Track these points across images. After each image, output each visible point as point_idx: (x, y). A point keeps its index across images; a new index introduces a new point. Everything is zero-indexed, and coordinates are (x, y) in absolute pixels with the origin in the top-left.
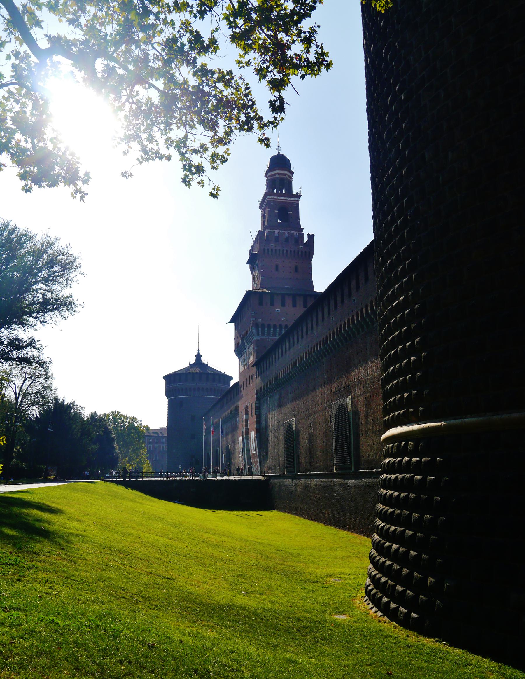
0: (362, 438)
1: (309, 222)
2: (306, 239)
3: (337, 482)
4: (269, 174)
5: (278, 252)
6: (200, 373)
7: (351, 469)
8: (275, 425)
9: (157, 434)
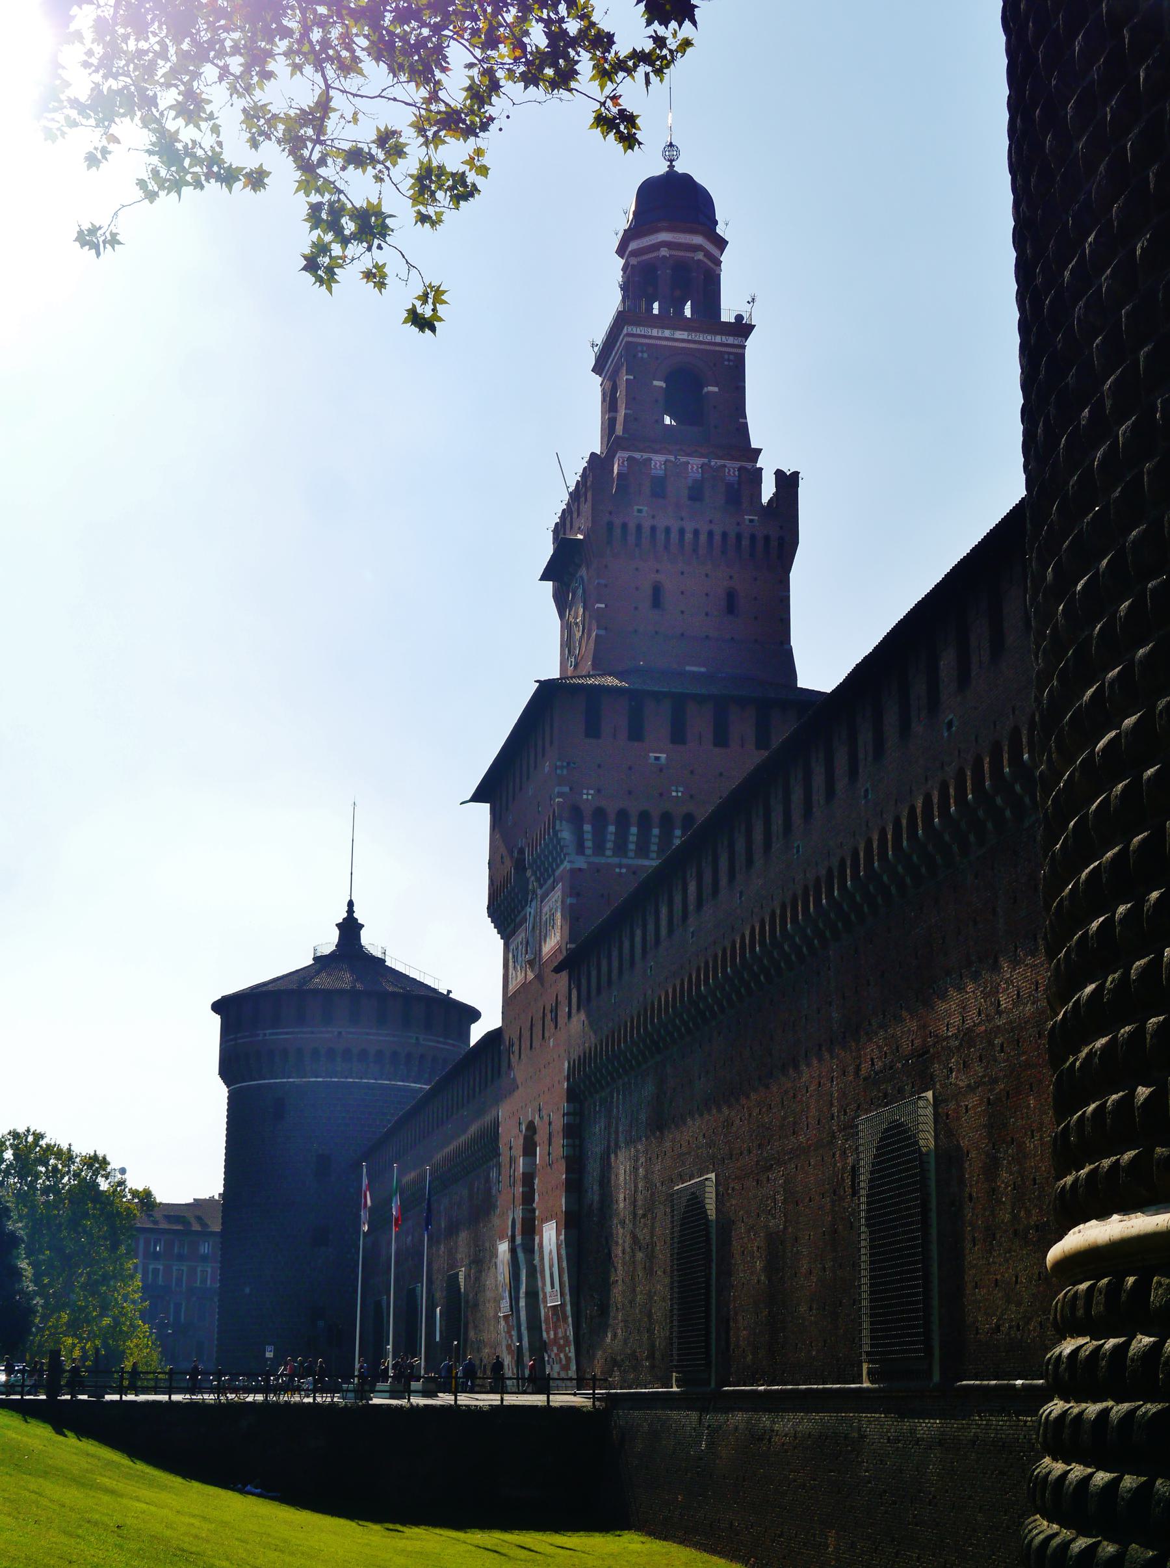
0: (973, 1255)
1: (780, 426)
2: (768, 489)
3: (875, 1425)
4: (633, 246)
5: (661, 536)
6: (353, 994)
8: (640, 1197)
9: (186, 1219)
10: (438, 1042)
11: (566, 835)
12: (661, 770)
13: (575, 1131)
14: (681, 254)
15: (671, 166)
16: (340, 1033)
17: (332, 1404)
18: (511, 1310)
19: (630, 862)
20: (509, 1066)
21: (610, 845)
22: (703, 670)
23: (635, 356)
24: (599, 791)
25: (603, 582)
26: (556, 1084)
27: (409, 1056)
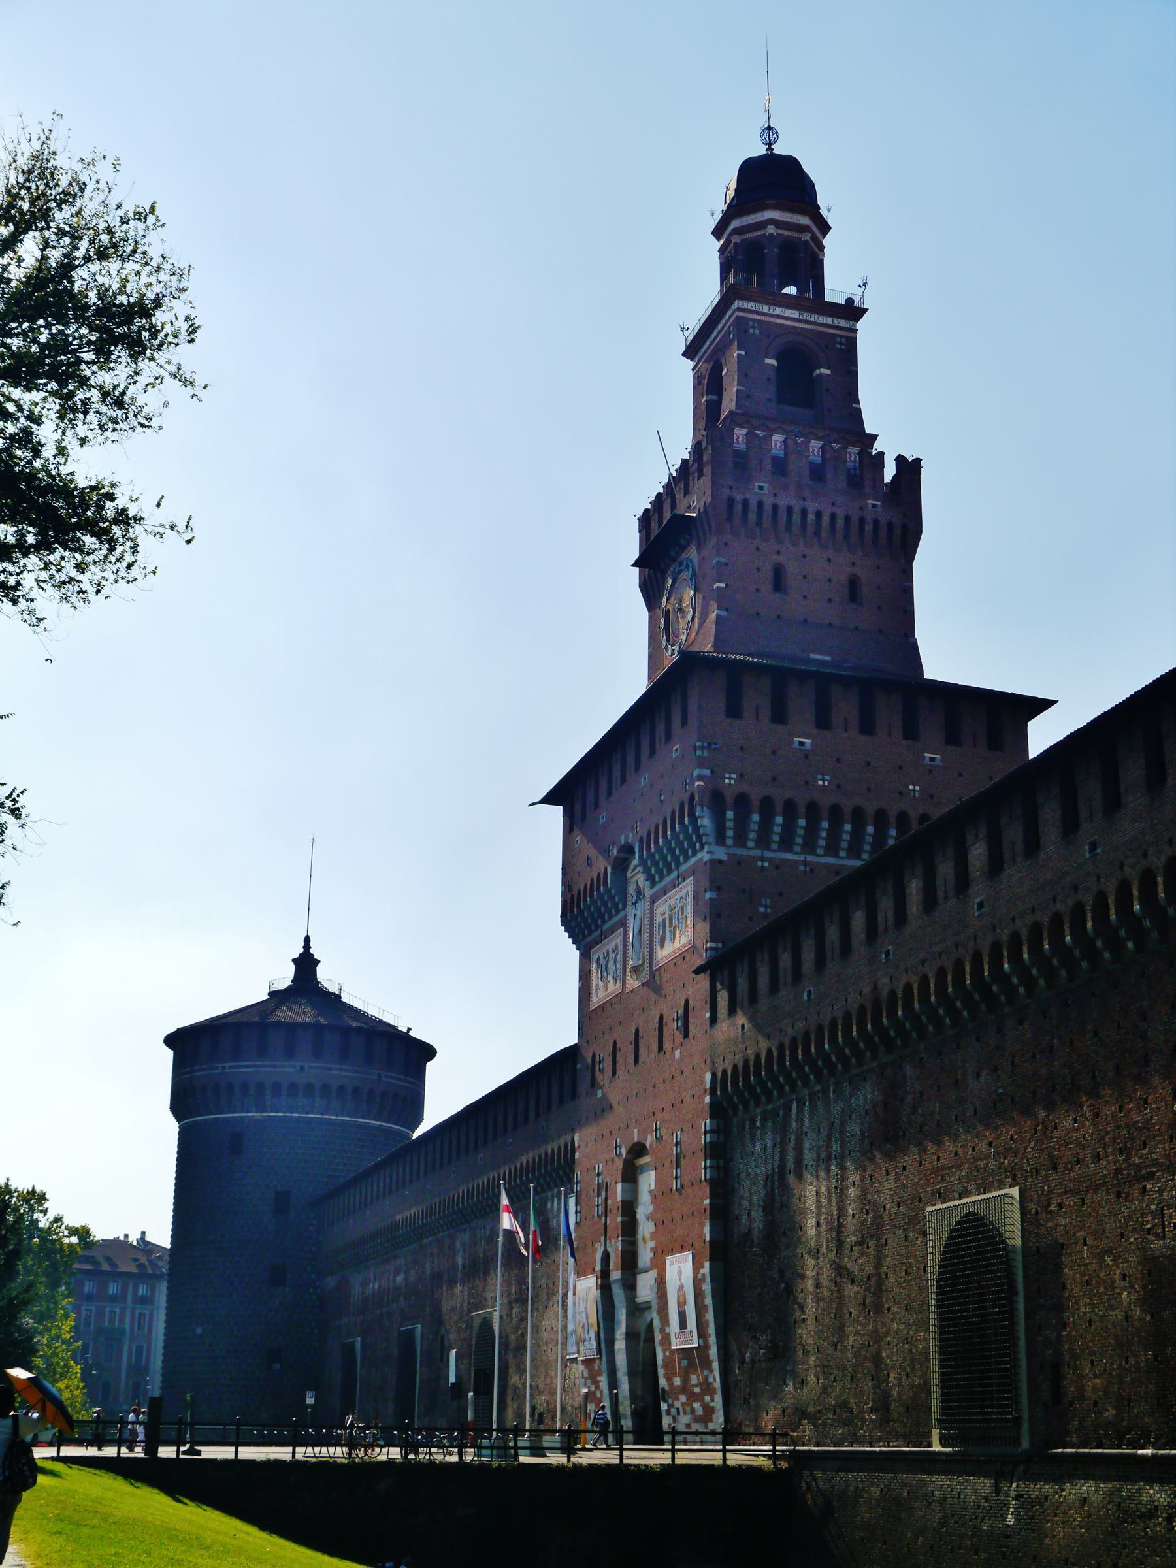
4: (735, 224)
5: (782, 515)
6: (316, 1028)
7: (1017, 1441)
8: (850, 1224)
9: (127, 1257)
10: (398, 1079)
11: (706, 822)
12: (806, 756)
13: (720, 1151)
14: (786, 233)
15: (770, 149)
16: (302, 1068)
17: (461, 1463)
18: (599, 1351)
19: (773, 855)
20: (594, 1084)
21: (752, 835)
22: (828, 658)
23: (746, 332)
24: (741, 775)
25: (723, 560)
26: (688, 1099)
27: (356, 1090)
